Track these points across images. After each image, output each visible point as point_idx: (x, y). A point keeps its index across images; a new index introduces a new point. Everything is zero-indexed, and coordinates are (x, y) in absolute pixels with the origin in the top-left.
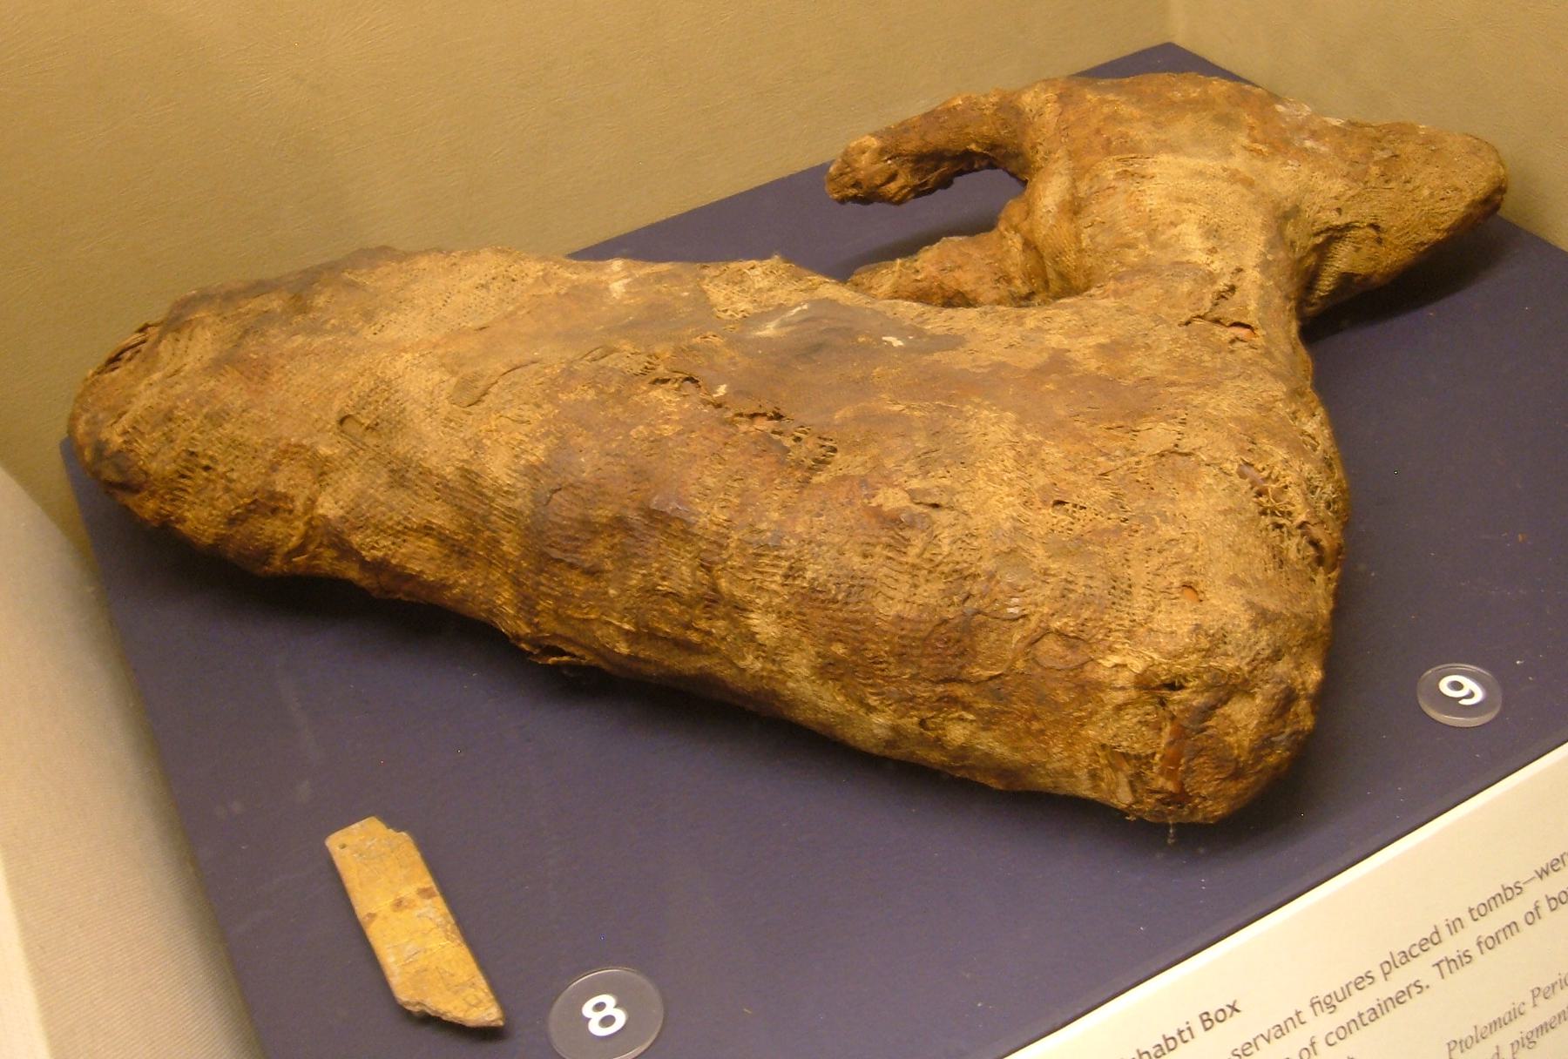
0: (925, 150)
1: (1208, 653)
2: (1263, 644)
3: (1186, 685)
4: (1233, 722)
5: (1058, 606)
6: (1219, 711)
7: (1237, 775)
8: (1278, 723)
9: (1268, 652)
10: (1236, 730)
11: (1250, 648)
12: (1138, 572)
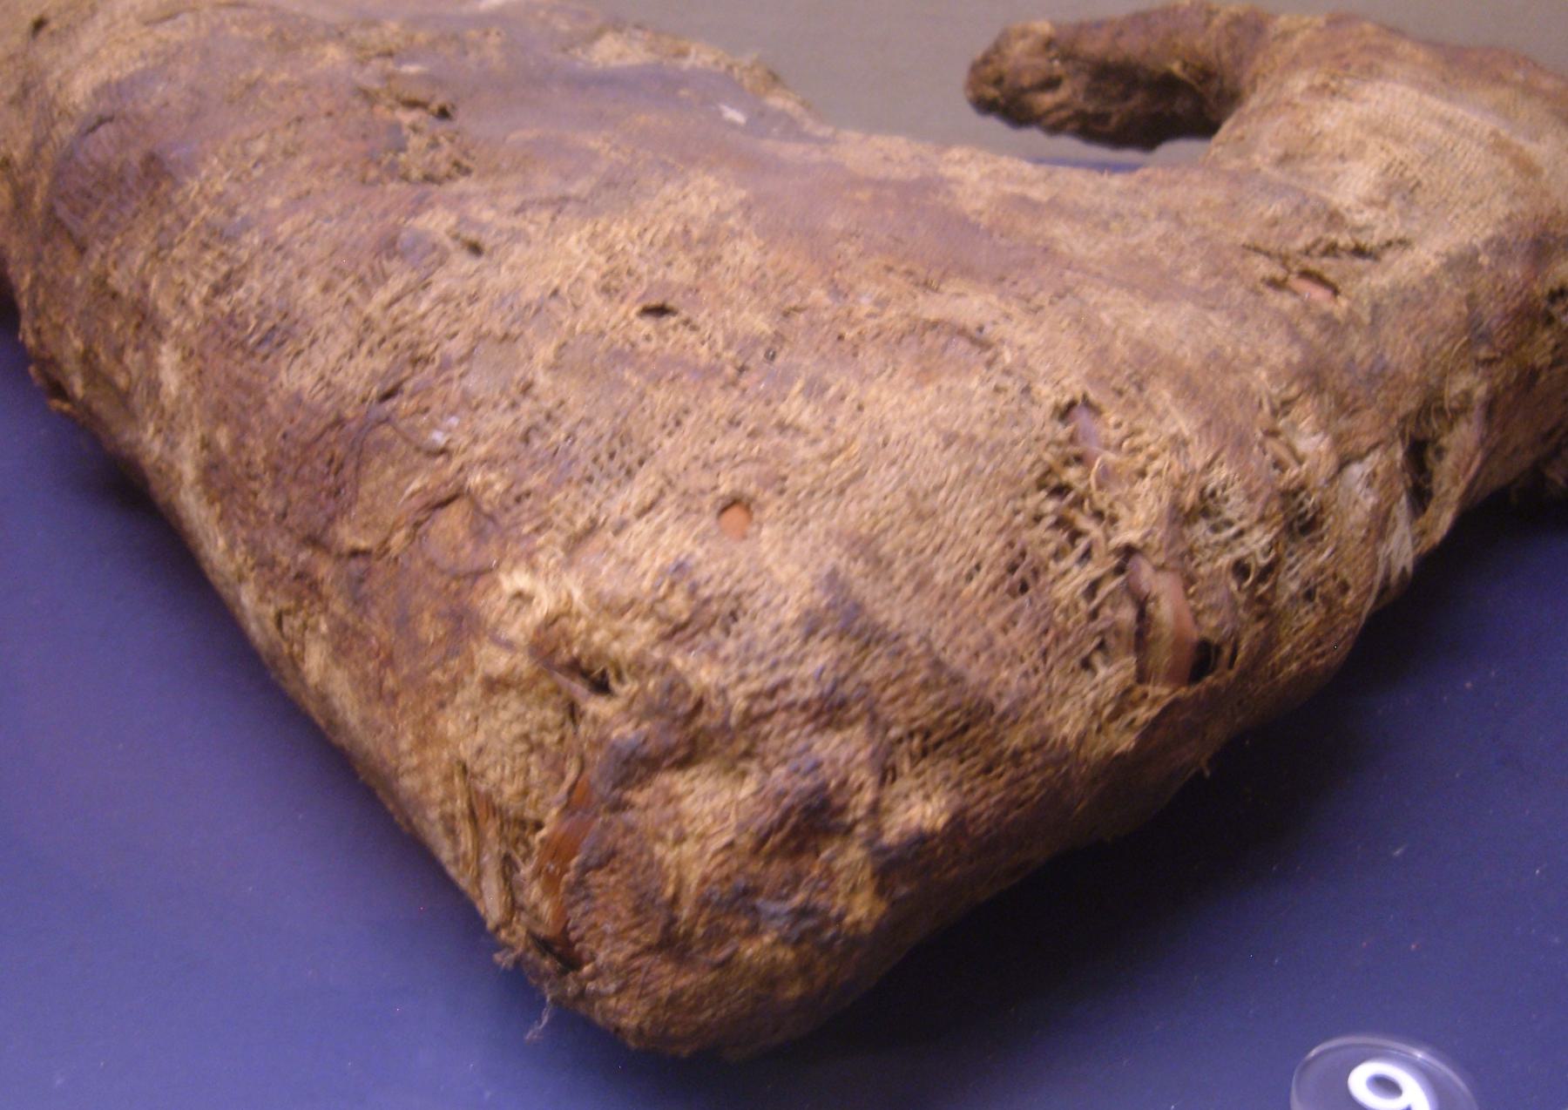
0: (1111, 59)
1: (675, 632)
2: (811, 667)
3: (613, 684)
4: (677, 816)
5: (504, 451)
6: (664, 779)
7: (672, 945)
8: (778, 870)
9: (810, 692)
10: (680, 839)
11: (774, 666)
12: (674, 452)
